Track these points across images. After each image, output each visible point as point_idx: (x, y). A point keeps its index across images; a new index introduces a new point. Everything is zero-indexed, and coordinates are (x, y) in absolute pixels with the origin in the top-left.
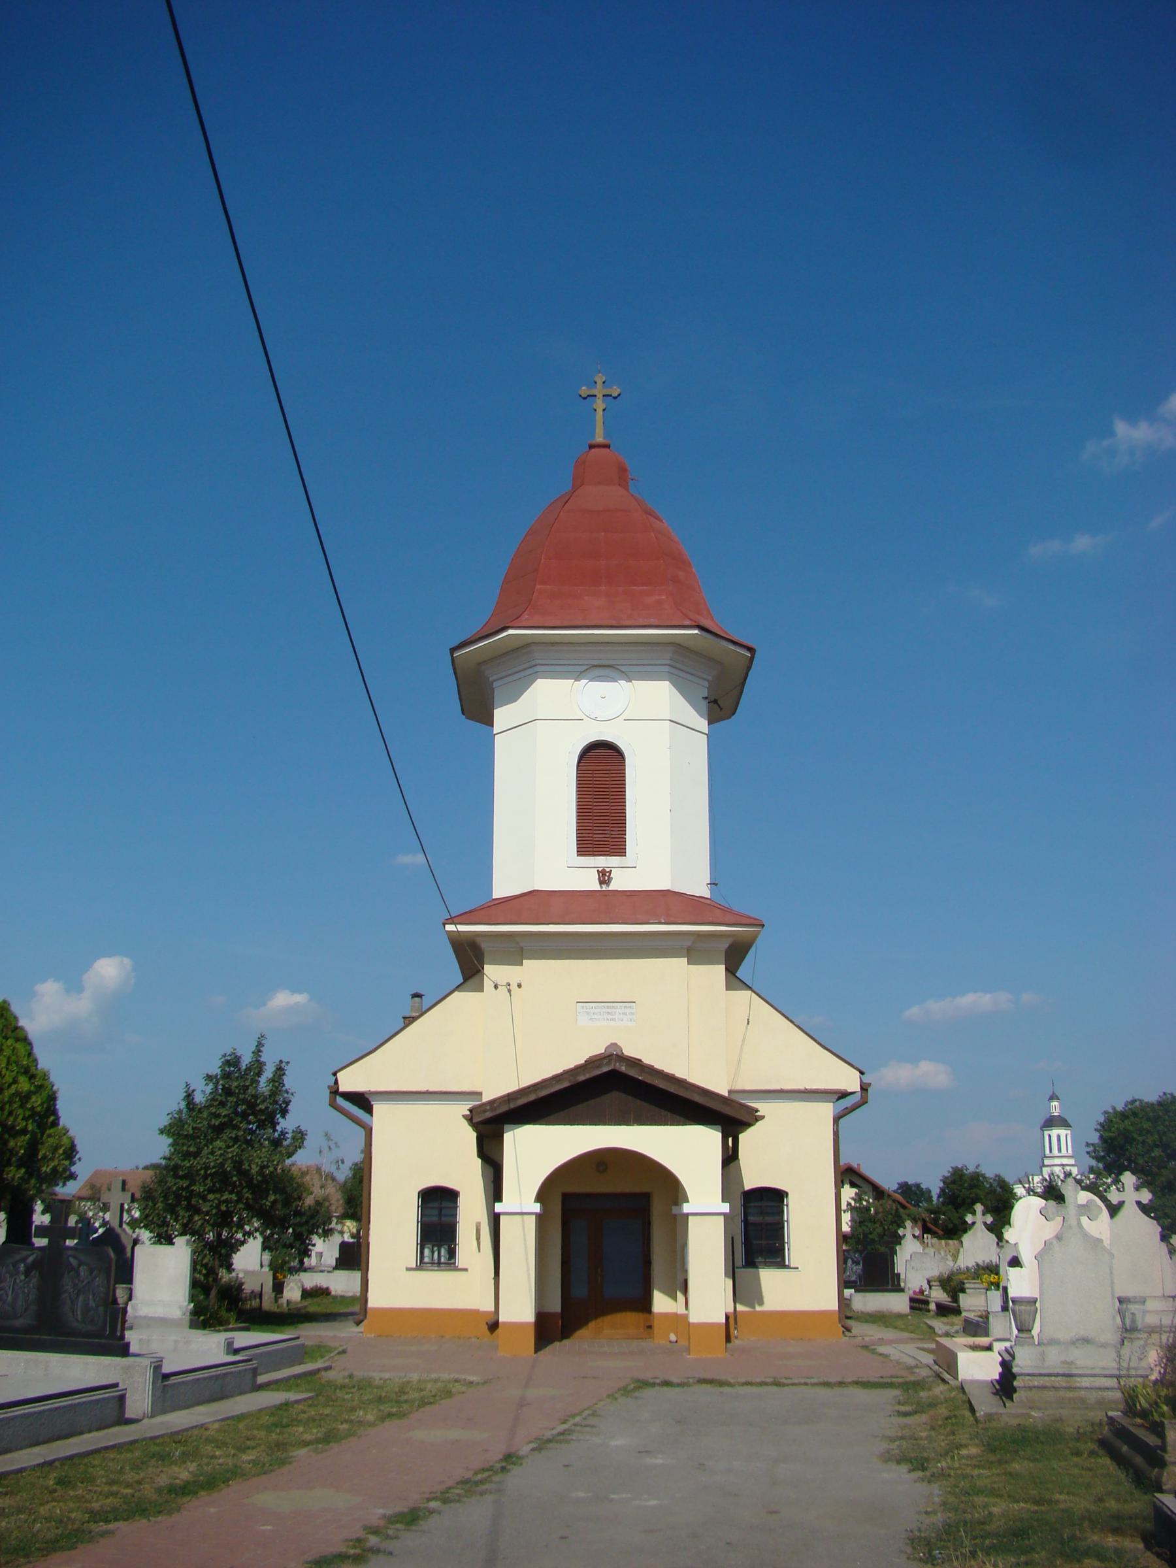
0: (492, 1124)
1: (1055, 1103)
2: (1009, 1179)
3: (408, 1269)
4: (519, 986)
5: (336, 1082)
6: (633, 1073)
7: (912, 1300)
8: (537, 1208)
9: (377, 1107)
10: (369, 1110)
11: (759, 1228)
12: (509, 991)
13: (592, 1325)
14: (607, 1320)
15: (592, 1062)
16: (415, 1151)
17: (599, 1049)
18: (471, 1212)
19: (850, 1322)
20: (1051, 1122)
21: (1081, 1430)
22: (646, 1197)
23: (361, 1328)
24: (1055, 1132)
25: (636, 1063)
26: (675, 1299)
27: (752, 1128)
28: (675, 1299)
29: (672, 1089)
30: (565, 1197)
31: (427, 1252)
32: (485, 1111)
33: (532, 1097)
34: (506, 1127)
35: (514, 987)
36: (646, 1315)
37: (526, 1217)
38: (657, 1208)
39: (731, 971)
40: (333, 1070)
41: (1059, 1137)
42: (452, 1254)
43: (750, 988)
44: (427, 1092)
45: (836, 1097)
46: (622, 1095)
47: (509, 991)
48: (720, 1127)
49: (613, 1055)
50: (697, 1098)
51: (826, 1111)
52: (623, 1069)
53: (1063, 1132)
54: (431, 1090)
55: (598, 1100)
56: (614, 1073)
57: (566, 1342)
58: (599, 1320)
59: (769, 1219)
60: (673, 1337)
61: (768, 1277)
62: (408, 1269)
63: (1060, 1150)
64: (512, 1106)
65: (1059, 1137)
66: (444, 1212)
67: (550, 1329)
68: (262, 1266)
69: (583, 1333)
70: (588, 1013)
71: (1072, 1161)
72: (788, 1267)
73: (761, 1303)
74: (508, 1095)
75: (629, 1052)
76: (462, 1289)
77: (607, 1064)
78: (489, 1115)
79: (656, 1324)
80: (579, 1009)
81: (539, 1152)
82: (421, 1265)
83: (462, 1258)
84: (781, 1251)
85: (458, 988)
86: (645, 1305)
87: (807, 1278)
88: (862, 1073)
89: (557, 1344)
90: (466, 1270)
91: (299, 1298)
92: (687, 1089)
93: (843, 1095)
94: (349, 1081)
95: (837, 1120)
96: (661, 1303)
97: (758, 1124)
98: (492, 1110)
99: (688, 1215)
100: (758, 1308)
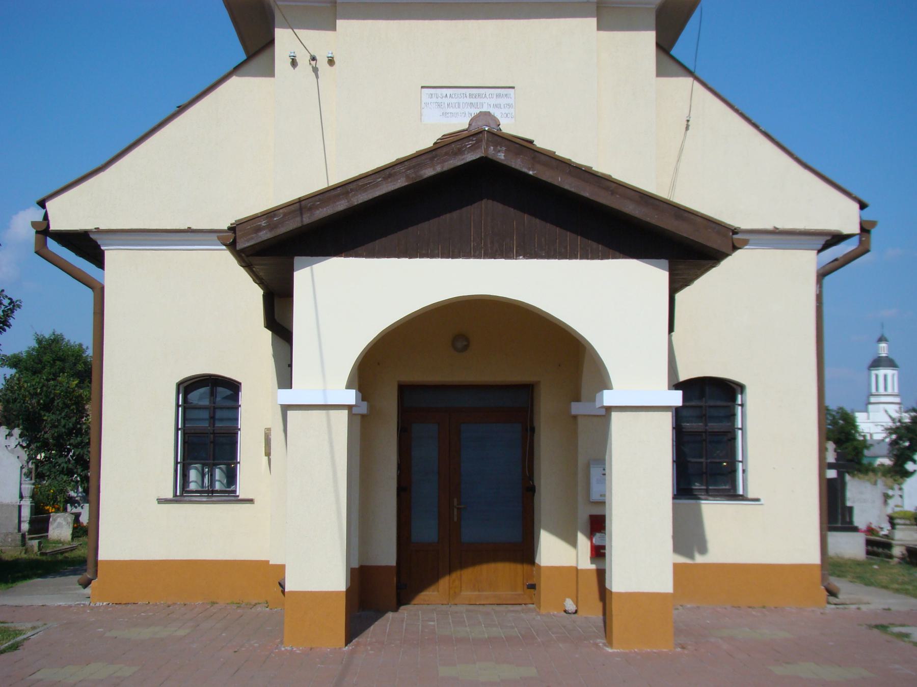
0: (274, 250)
1: (883, 345)
2: (848, 409)
3: (161, 501)
4: (331, 62)
5: (46, 217)
6: (518, 164)
7: (869, 543)
8: (350, 397)
9: (111, 256)
10: (98, 259)
11: (707, 437)
12: (315, 70)
13: (444, 582)
14: (468, 574)
15: (448, 145)
16: (169, 320)
17: (459, 123)
18: (254, 416)
19: (836, 582)
20: (878, 363)
21: (8, 377)
22: (526, 392)
23: (88, 591)
24: (882, 372)
25: (523, 146)
26: (573, 543)
27: (729, 258)
28: (573, 543)
29: (586, 191)
30: (404, 390)
31: (193, 474)
32: (258, 229)
33: (342, 205)
34: (297, 260)
35: (322, 63)
36: (526, 567)
37: (333, 413)
38: (546, 408)
39: (664, 47)
40: (40, 197)
41: (885, 376)
42: (231, 477)
43: (690, 73)
44: (190, 231)
45: (821, 241)
46: (499, 207)
47: (315, 70)
48: (665, 262)
49: (483, 133)
50: (630, 208)
51: (807, 261)
52: (501, 156)
53: (889, 372)
54: (194, 227)
55: (455, 214)
56: (485, 166)
57: (405, 611)
58: (455, 575)
59: (714, 426)
60: (570, 605)
61: (714, 512)
62: (161, 501)
63: (886, 388)
64: (307, 219)
65: (885, 376)
66: (219, 414)
67: (371, 595)
68: (21, 497)
69: (428, 595)
70: (439, 105)
71: (897, 400)
72: (743, 498)
73: (703, 550)
74: (300, 201)
75: (509, 127)
76: (206, 534)
77: (474, 148)
78: (265, 235)
79: (544, 585)
80: (425, 99)
81: (358, 299)
82: (183, 493)
83: (243, 488)
84: (731, 473)
85: (237, 70)
86: (525, 552)
87: (774, 517)
88: (863, 206)
89: (390, 615)
90: (251, 501)
91: (69, 537)
92: (613, 193)
93: (836, 238)
94: (67, 214)
95: (822, 275)
96: (552, 551)
97: (738, 253)
98: (271, 227)
99: (609, 409)
100: (699, 559)
